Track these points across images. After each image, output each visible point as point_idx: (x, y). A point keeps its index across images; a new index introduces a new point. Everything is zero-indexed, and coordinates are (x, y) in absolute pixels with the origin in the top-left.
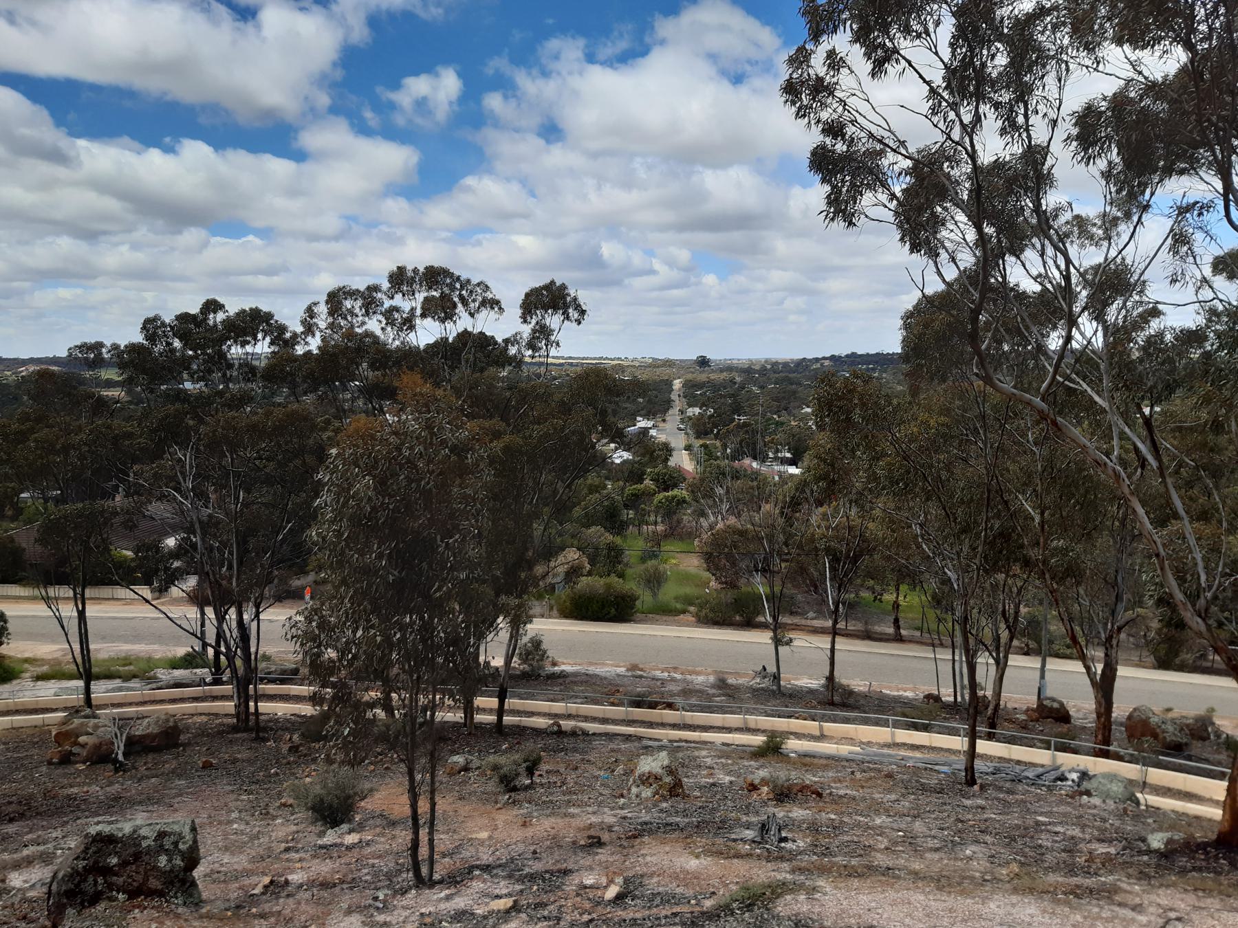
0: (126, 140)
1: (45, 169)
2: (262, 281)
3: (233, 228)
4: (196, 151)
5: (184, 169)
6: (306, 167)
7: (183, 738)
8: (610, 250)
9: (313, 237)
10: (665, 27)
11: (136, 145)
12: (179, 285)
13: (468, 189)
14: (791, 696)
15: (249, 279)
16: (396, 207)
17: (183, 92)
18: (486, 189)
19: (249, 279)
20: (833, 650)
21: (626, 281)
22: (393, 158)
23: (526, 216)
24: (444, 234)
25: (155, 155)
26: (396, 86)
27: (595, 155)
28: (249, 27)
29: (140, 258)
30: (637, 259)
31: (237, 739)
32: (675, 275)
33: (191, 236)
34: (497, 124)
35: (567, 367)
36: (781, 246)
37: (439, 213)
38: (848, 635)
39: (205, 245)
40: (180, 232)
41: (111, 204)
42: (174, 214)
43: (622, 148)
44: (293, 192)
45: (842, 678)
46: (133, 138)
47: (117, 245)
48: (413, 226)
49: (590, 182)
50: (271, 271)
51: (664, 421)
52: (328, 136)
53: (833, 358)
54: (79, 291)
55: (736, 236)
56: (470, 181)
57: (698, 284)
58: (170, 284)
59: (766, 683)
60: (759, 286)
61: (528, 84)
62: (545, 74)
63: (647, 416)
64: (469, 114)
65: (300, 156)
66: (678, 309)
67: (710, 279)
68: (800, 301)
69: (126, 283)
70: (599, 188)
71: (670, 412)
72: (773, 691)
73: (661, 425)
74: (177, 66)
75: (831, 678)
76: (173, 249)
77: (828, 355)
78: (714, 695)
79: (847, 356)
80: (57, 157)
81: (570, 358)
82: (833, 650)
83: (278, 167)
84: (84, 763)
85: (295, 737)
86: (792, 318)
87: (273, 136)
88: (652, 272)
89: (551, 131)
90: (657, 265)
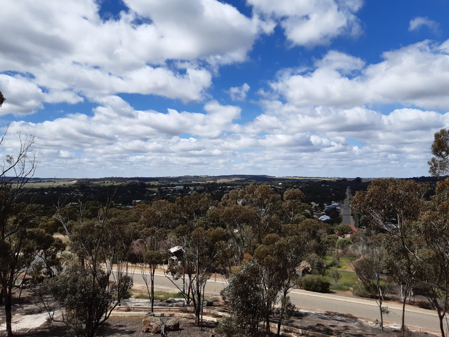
0: (151, 110)
1: (128, 120)
2: (197, 152)
3: (187, 136)
4: (173, 112)
5: (171, 119)
6: (207, 116)
7: (180, 327)
8: (314, 139)
9: (211, 138)
10: (318, 63)
11: (156, 112)
12: (172, 154)
13: (257, 120)
14: (388, 332)
15: (192, 152)
16: (236, 127)
17: (167, 95)
18: (264, 120)
19: (192, 152)
20: (404, 310)
21: (321, 149)
22: (232, 111)
23: (279, 128)
24: (253, 135)
25: (161, 115)
26: (228, 88)
27: (299, 107)
28: (185, 76)
29: (160, 146)
30: (325, 141)
31: (196, 329)
32: (340, 146)
33: (175, 139)
34: (263, 98)
35: (304, 181)
36: (381, 135)
37: (250, 129)
38: (412, 303)
39: (179, 141)
40: (171, 138)
41: (149, 129)
42: (170, 133)
43: (311, 103)
44: (203, 124)
45: (408, 325)
46: (153, 109)
47: (152, 142)
48: (242, 133)
49: (300, 116)
50: (199, 149)
51: (343, 203)
52: (212, 106)
53: (414, 178)
54: (143, 156)
55: (363, 133)
56: (258, 118)
57: (351, 149)
58: (169, 154)
59: (378, 326)
60: (375, 150)
61: (274, 86)
62: (277, 81)
63: (336, 201)
64: (251, 95)
65: (205, 113)
66: (344, 159)
67: (355, 148)
68: (394, 156)
69: (156, 154)
70: (303, 117)
71: (346, 199)
72: (380, 330)
73: (342, 204)
74: (164, 88)
75: (403, 325)
76: (169, 143)
77: (412, 177)
78: (357, 330)
79: (420, 177)
80: (131, 116)
81: (306, 177)
82: (404, 310)
83: (199, 116)
84: (153, 333)
85: (213, 331)
86: (393, 162)
87: (195, 107)
88: (331, 146)
89: (283, 100)
90: (333, 143)
